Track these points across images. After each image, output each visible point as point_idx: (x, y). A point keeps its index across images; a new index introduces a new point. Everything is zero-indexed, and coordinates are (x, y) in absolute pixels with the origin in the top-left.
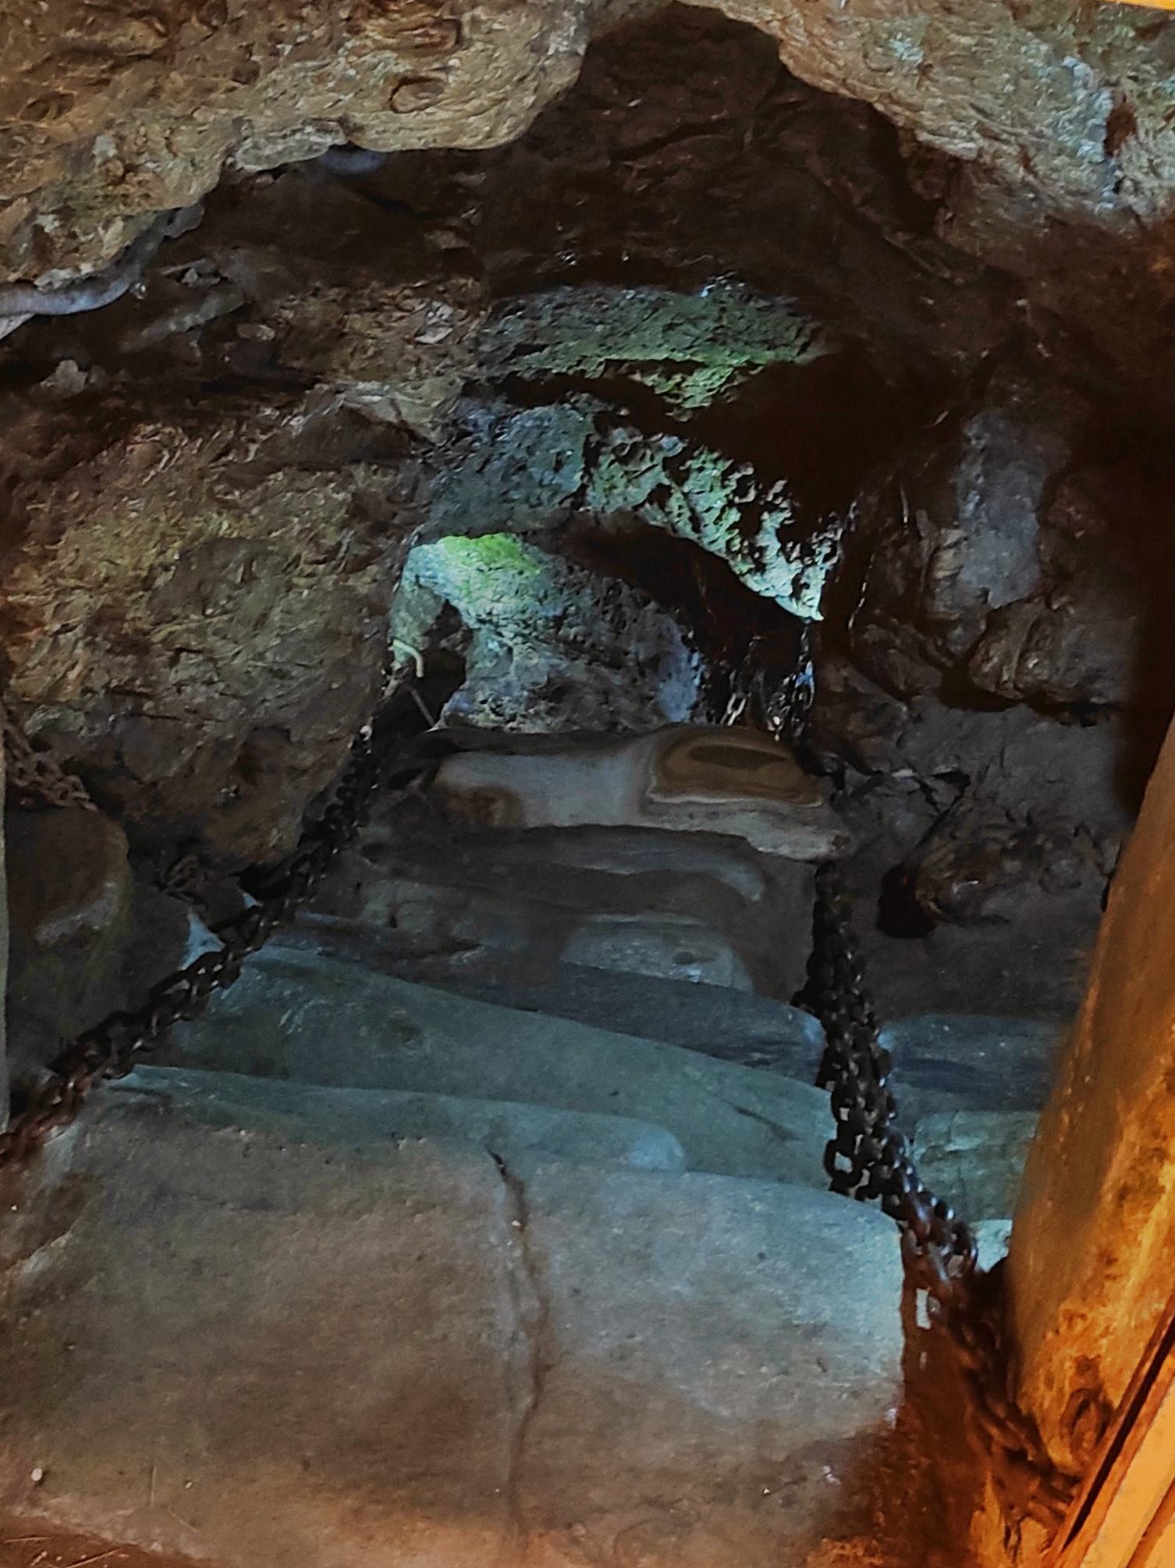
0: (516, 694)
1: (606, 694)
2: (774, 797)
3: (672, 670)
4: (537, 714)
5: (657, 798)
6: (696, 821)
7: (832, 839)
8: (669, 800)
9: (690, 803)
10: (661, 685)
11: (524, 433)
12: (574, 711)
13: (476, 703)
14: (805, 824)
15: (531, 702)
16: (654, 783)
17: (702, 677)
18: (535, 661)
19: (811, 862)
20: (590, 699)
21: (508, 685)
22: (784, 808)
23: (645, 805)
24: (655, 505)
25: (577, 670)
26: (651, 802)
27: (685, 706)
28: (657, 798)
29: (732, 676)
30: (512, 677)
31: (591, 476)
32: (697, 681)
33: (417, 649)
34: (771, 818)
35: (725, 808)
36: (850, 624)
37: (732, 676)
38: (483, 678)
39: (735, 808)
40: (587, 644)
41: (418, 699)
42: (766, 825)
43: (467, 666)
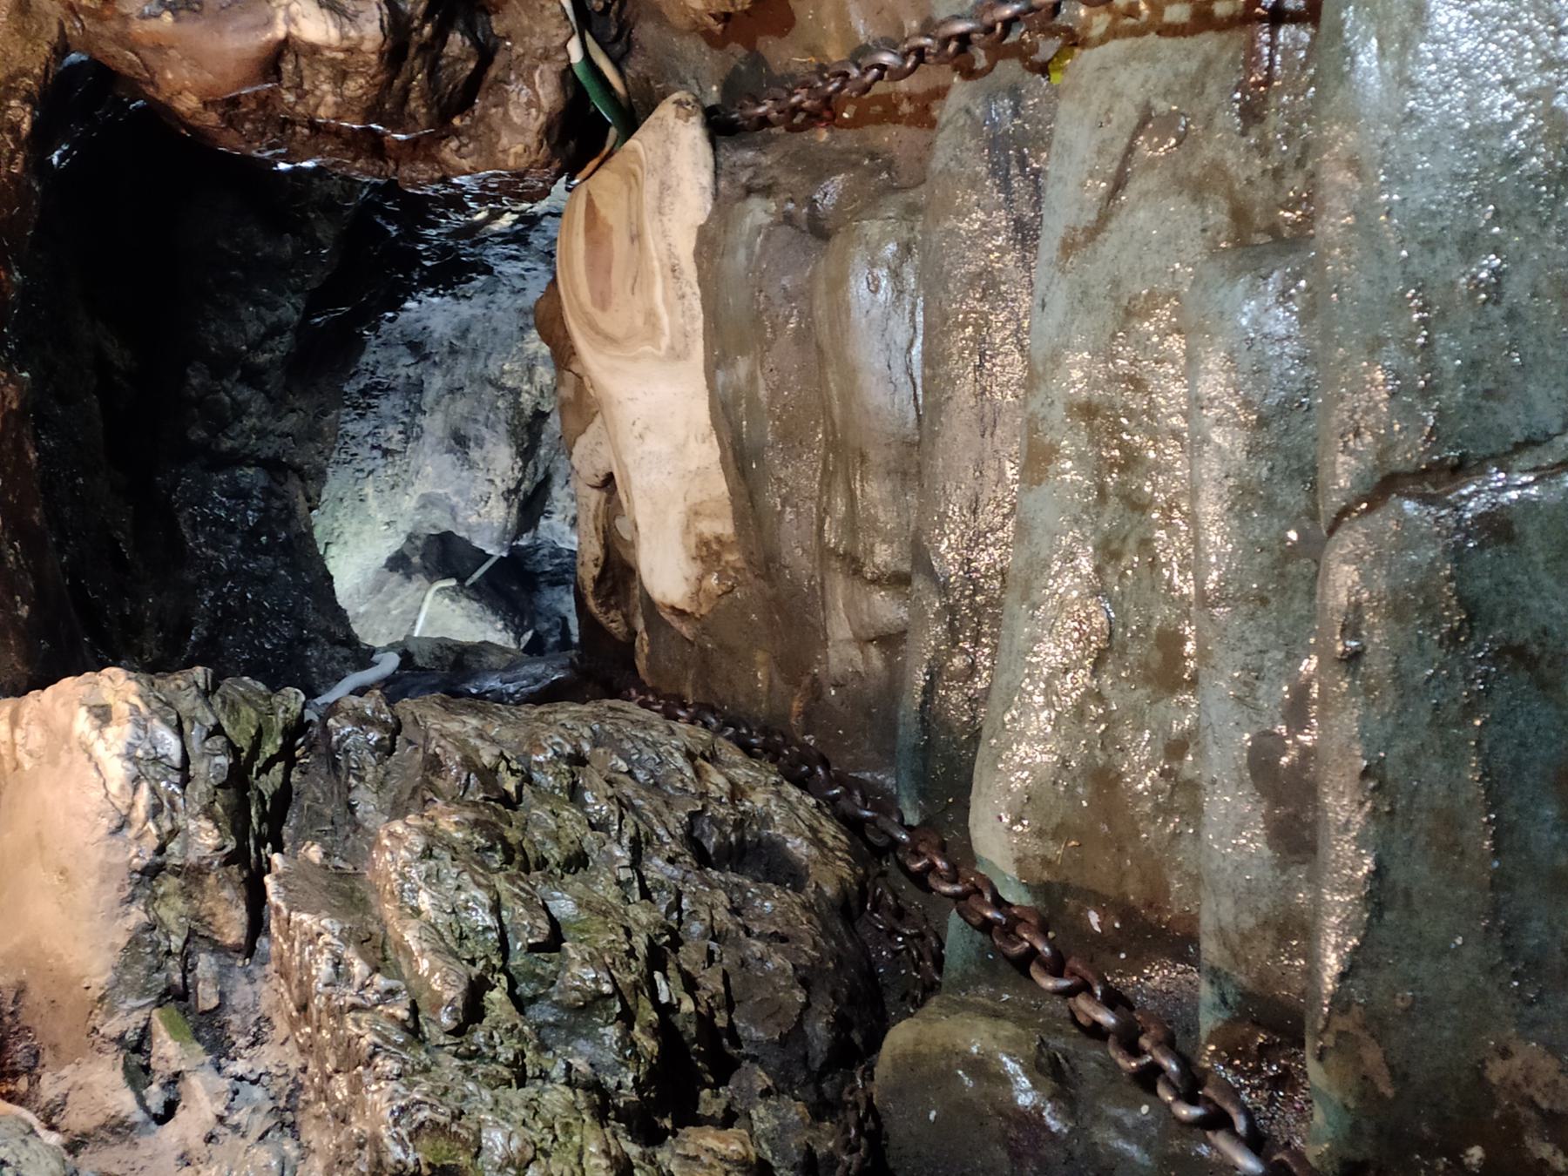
0: (466, 483)
1: (455, 391)
2: (640, 199)
3: (419, 326)
4: (484, 459)
5: (665, 342)
6: (688, 290)
7: (680, 122)
8: (667, 331)
9: (665, 300)
10: (436, 335)
11: (214, 542)
12: (476, 421)
13: (486, 523)
14: (668, 159)
15: (472, 466)
16: (648, 348)
17: (431, 296)
18: (429, 469)
19: (715, 148)
20: (462, 406)
21: (459, 493)
22: (650, 186)
23: (677, 354)
24: (265, 377)
25: (434, 424)
26: (672, 348)
27: (455, 308)
28: (665, 342)
29: (428, 263)
30: (449, 490)
31: (246, 456)
32: (436, 300)
33: (427, 590)
34: (668, 199)
35: (665, 259)
36: (402, 137)
37: (428, 263)
38: (454, 519)
39: (663, 246)
40: (406, 420)
41: (476, 575)
42: (678, 206)
43: (434, 532)
